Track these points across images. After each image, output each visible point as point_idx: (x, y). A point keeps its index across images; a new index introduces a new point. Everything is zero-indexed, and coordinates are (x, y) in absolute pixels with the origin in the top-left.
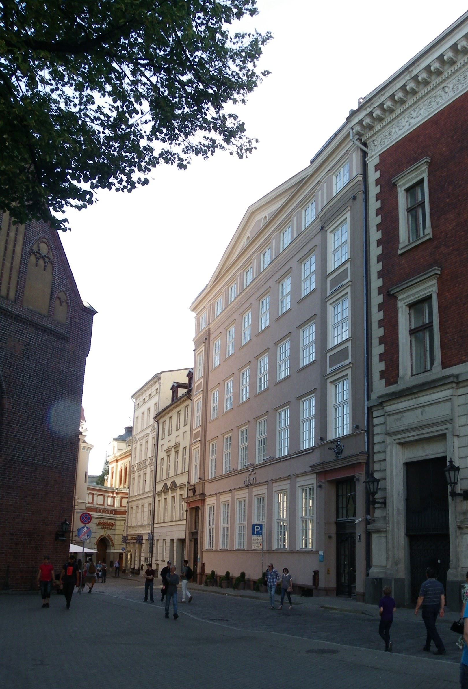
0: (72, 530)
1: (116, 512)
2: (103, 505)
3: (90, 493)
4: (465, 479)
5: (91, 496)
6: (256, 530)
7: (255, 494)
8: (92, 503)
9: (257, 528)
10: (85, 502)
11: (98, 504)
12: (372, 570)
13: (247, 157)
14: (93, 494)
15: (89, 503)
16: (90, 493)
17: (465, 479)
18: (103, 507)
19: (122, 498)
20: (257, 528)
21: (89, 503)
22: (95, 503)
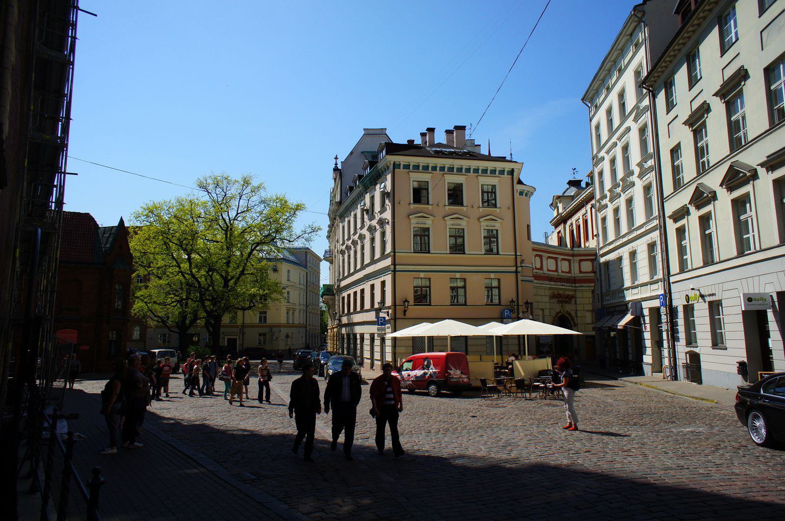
0: (63, 171)
1: (574, 281)
2: (556, 270)
3: (537, 255)
4: (496, 318)
5: (538, 259)
6: (380, 322)
7: (291, 272)
8: (541, 268)
9: (381, 320)
10: (531, 266)
11: (548, 270)
12: (568, 187)
13: (336, 158)
14: (541, 257)
15: (537, 269)
16: (537, 255)
17: (497, 318)
18: (569, 275)
19: (580, 261)
20: (381, 320)
21: (537, 269)
22: (545, 269)
